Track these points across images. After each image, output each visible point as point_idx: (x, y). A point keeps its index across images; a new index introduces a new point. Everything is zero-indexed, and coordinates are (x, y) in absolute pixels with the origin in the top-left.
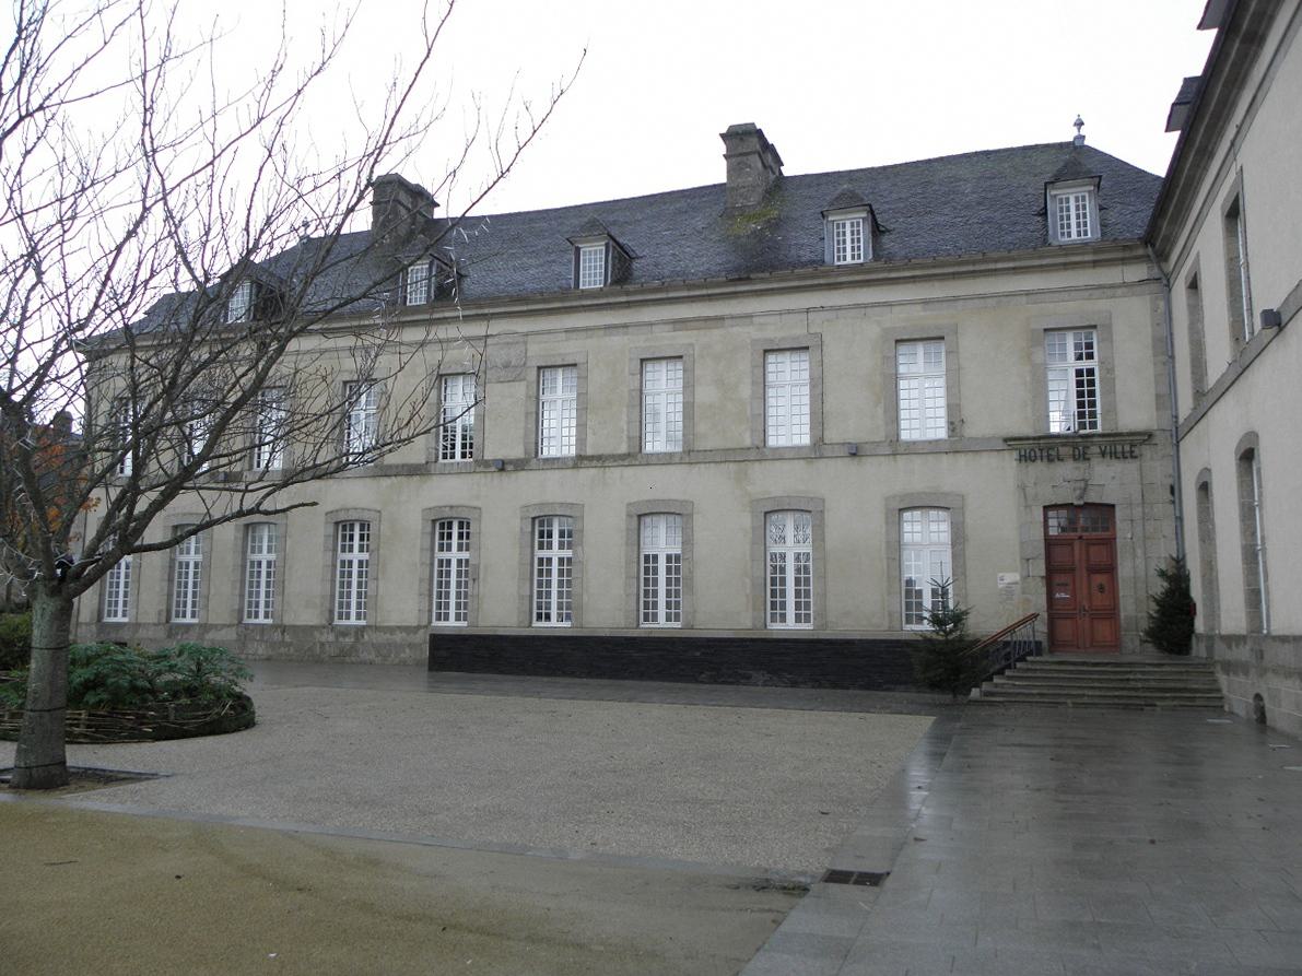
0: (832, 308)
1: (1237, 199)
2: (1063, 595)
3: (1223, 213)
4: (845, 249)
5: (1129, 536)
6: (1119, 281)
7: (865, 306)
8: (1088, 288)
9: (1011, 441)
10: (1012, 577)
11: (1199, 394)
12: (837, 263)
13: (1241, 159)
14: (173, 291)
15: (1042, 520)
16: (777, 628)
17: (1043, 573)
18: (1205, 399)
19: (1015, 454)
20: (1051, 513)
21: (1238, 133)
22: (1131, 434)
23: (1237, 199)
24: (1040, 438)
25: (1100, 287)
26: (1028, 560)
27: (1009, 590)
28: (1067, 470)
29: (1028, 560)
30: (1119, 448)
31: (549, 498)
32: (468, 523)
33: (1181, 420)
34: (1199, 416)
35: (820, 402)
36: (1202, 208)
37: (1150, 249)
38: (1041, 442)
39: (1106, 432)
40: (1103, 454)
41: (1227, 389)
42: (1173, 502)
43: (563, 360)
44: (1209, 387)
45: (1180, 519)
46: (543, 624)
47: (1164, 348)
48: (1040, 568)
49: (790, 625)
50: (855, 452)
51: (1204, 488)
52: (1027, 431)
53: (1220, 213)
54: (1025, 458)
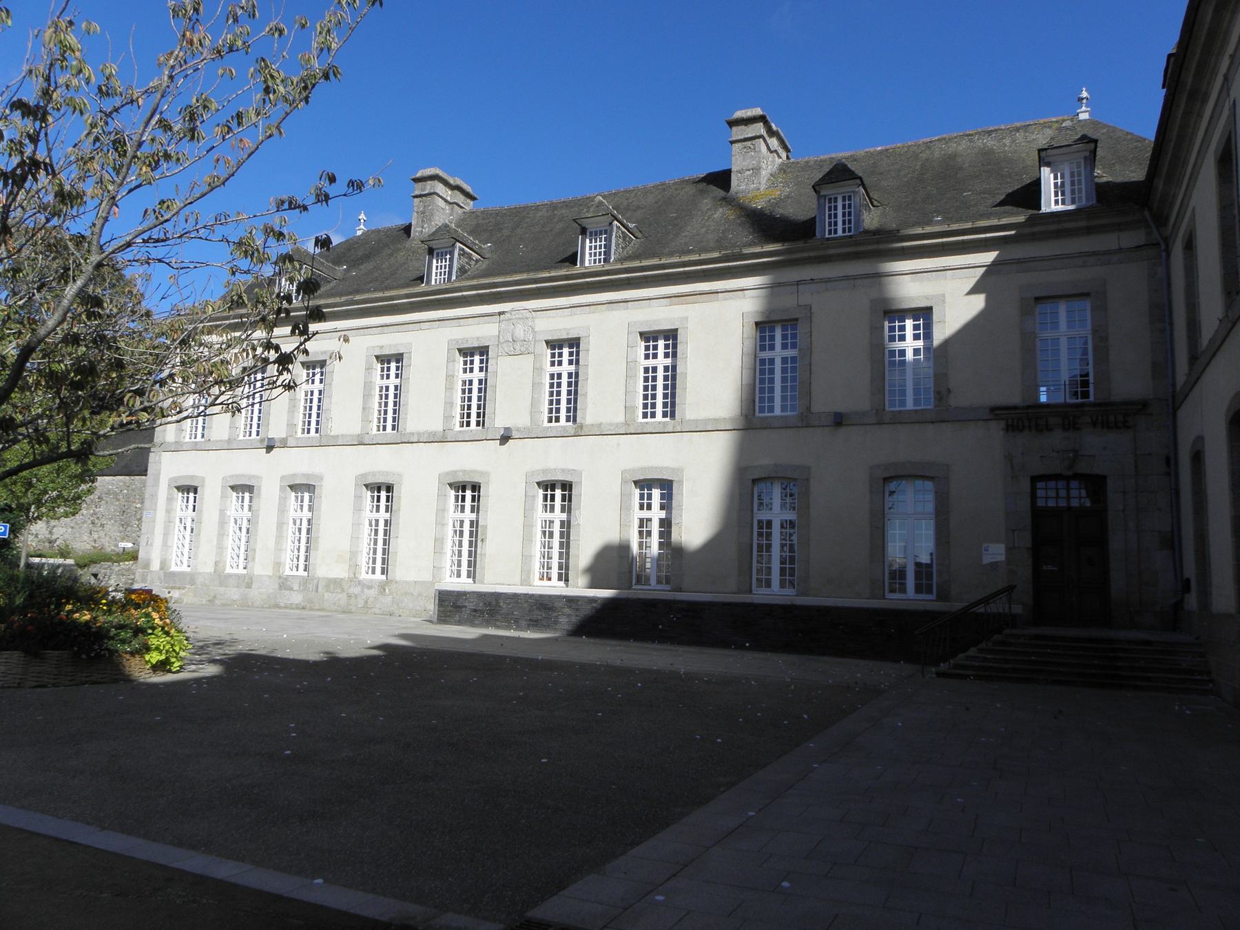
0: (822, 281)
1: (1229, 140)
2: (1050, 568)
3: (1216, 159)
4: (844, 222)
5: (1121, 507)
6: (1114, 246)
7: (855, 278)
8: (1081, 255)
9: (996, 412)
10: (996, 552)
11: (1193, 358)
12: (827, 236)
13: (1233, 94)
14: (1044, 505)
15: (1029, 490)
16: (760, 595)
17: (1029, 544)
18: (1199, 359)
19: (1002, 424)
20: (1039, 485)
21: (1231, 63)
22: (1126, 403)
23: (1229, 140)
24: (1028, 407)
25: (1094, 254)
26: (1014, 530)
27: (994, 566)
28: (1057, 439)
29: (1014, 530)
30: (1112, 418)
31: (552, 465)
32: (480, 487)
33: (1178, 388)
34: (1194, 380)
35: (808, 372)
36: (1197, 159)
37: (1146, 213)
38: (1030, 411)
39: (1098, 401)
40: (1094, 424)
41: (1218, 349)
42: (1168, 474)
43: (568, 334)
44: (1203, 349)
45: (1177, 492)
46: (764, 591)
47: (1161, 313)
48: (1026, 540)
49: (775, 592)
50: (839, 420)
51: (1198, 458)
52: (1016, 400)
53: (1213, 159)
54: (1012, 427)
